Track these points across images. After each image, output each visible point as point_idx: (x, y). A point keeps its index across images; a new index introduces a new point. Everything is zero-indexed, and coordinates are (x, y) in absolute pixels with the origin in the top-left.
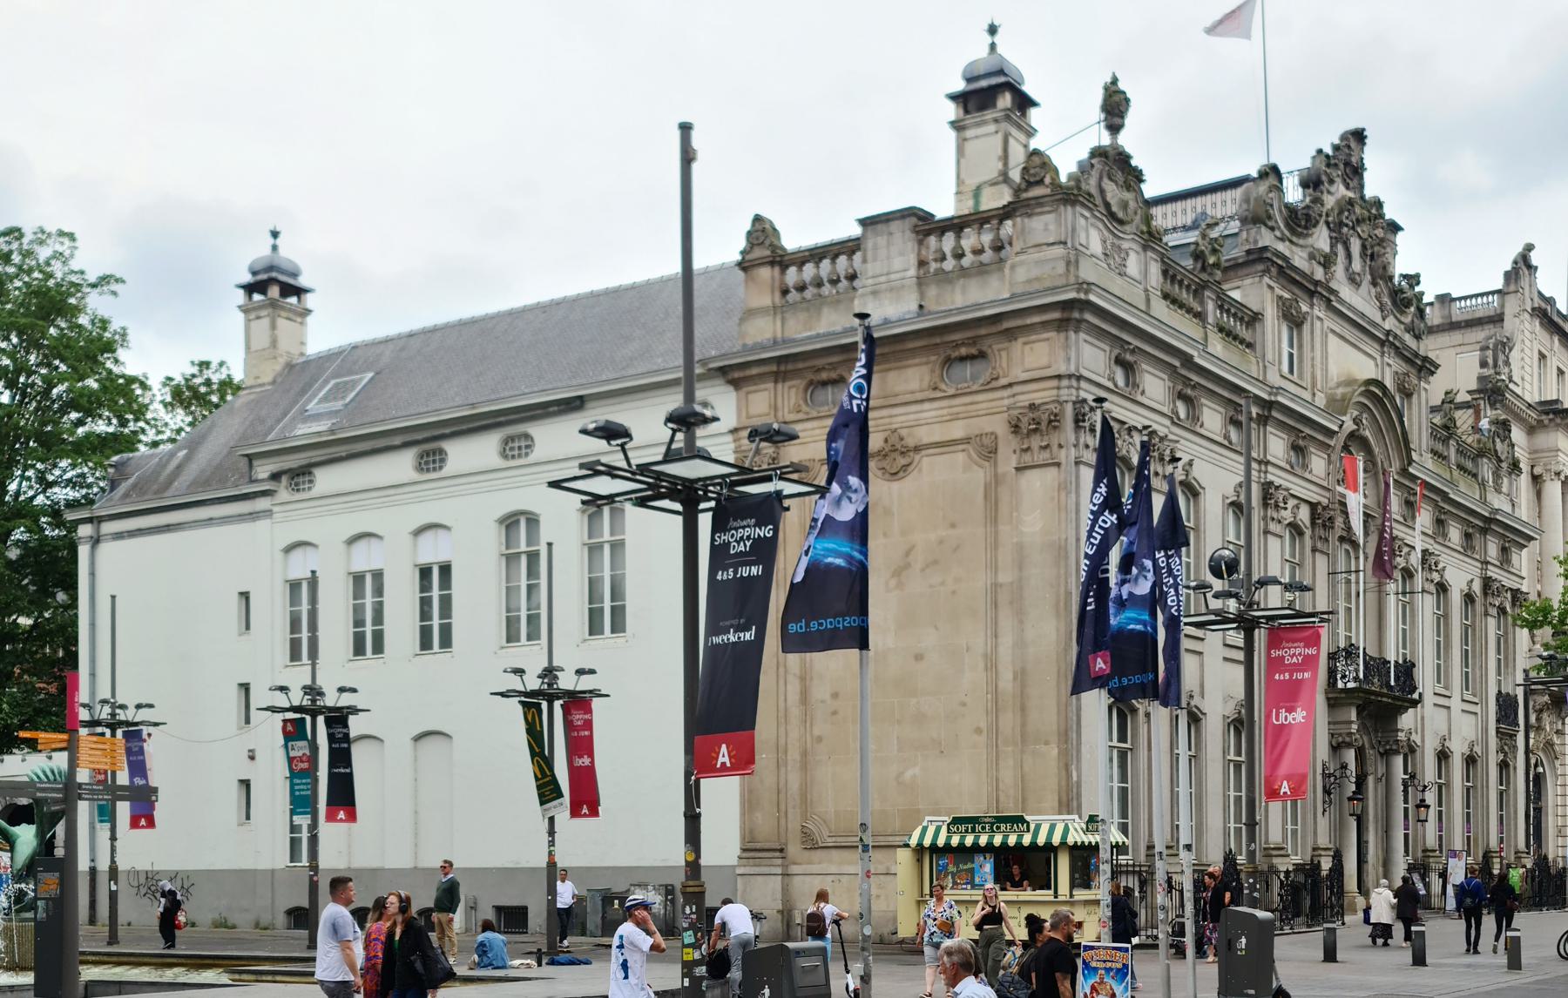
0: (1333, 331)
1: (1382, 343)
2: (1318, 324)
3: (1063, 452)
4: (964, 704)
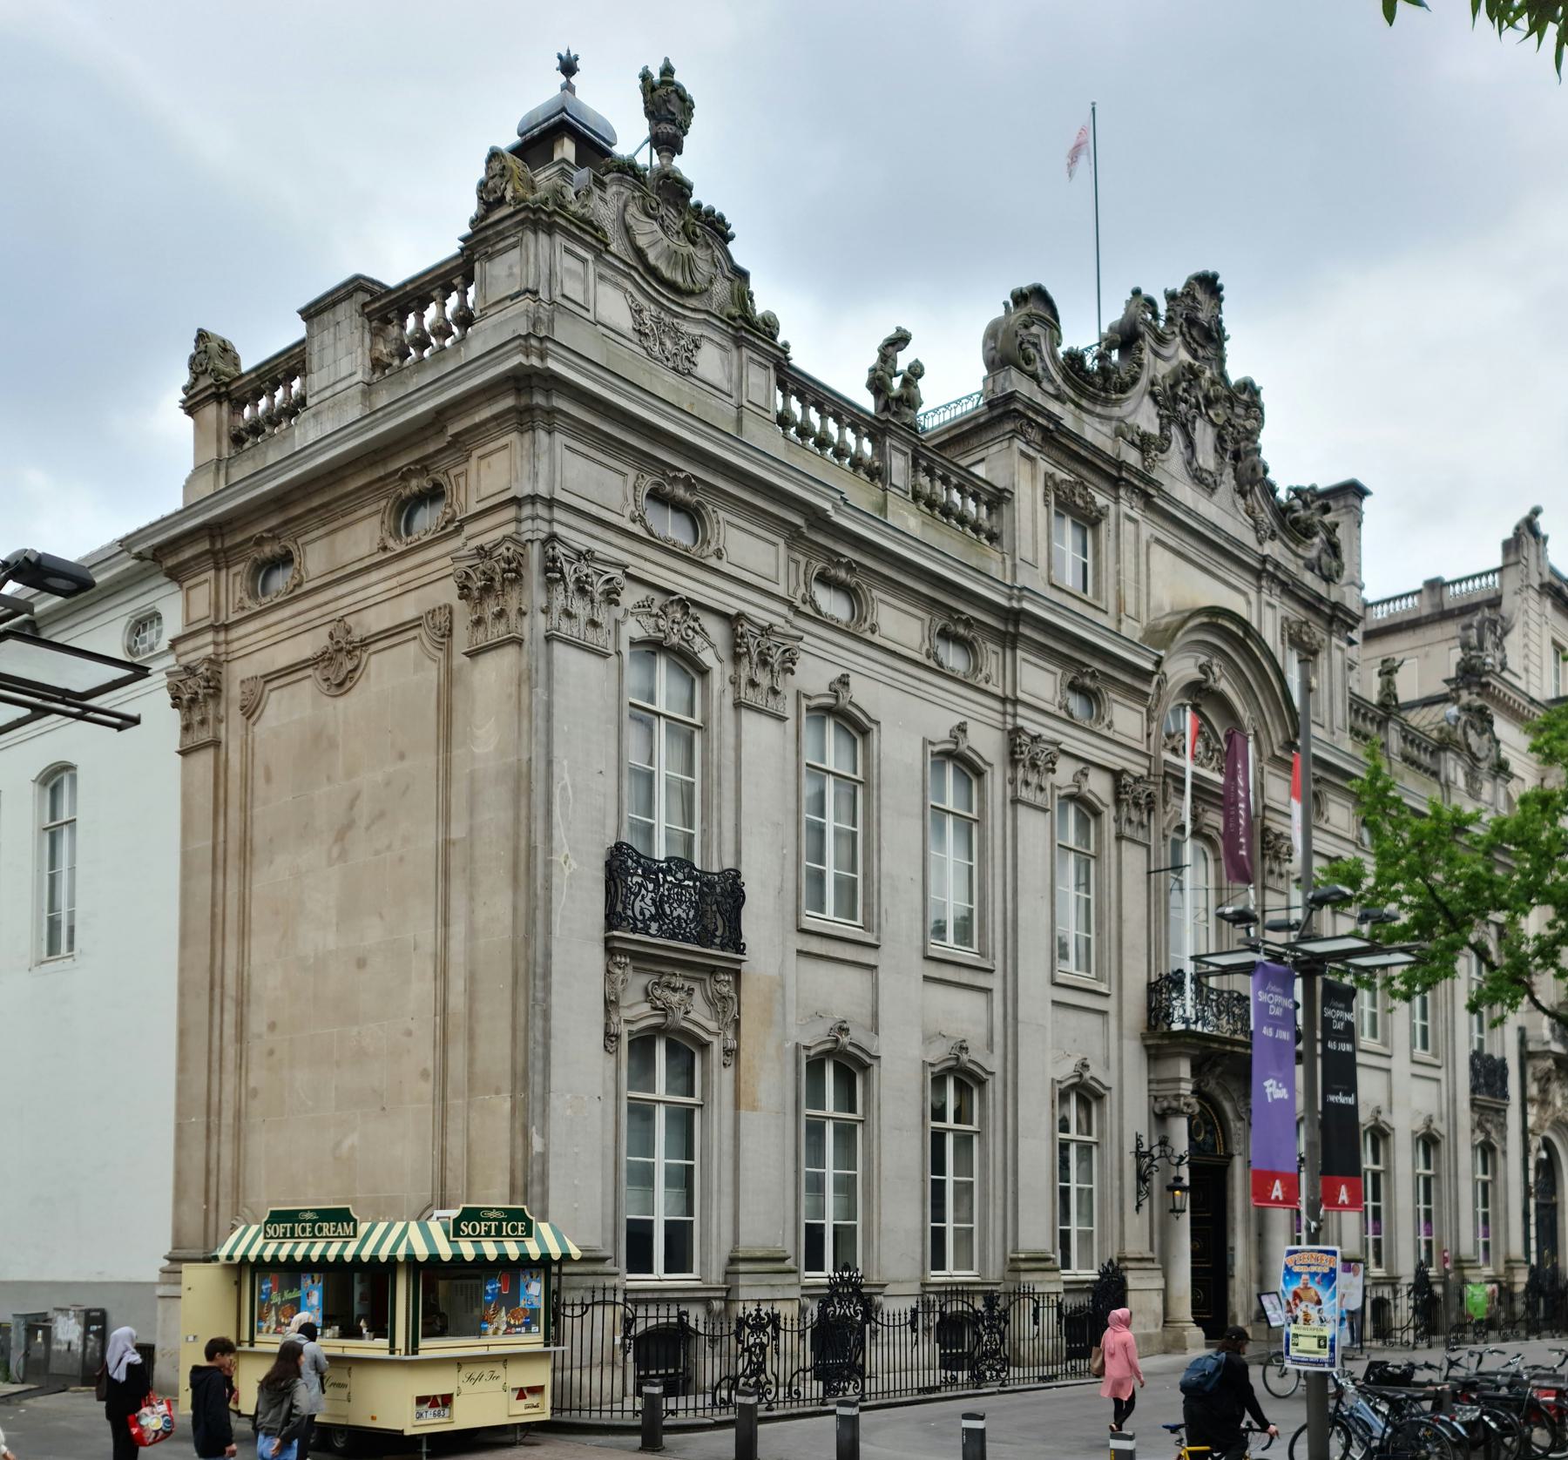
0: (1158, 541)
1: (1258, 574)
2: (1128, 527)
3: (526, 620)
4: (409, 1033)
